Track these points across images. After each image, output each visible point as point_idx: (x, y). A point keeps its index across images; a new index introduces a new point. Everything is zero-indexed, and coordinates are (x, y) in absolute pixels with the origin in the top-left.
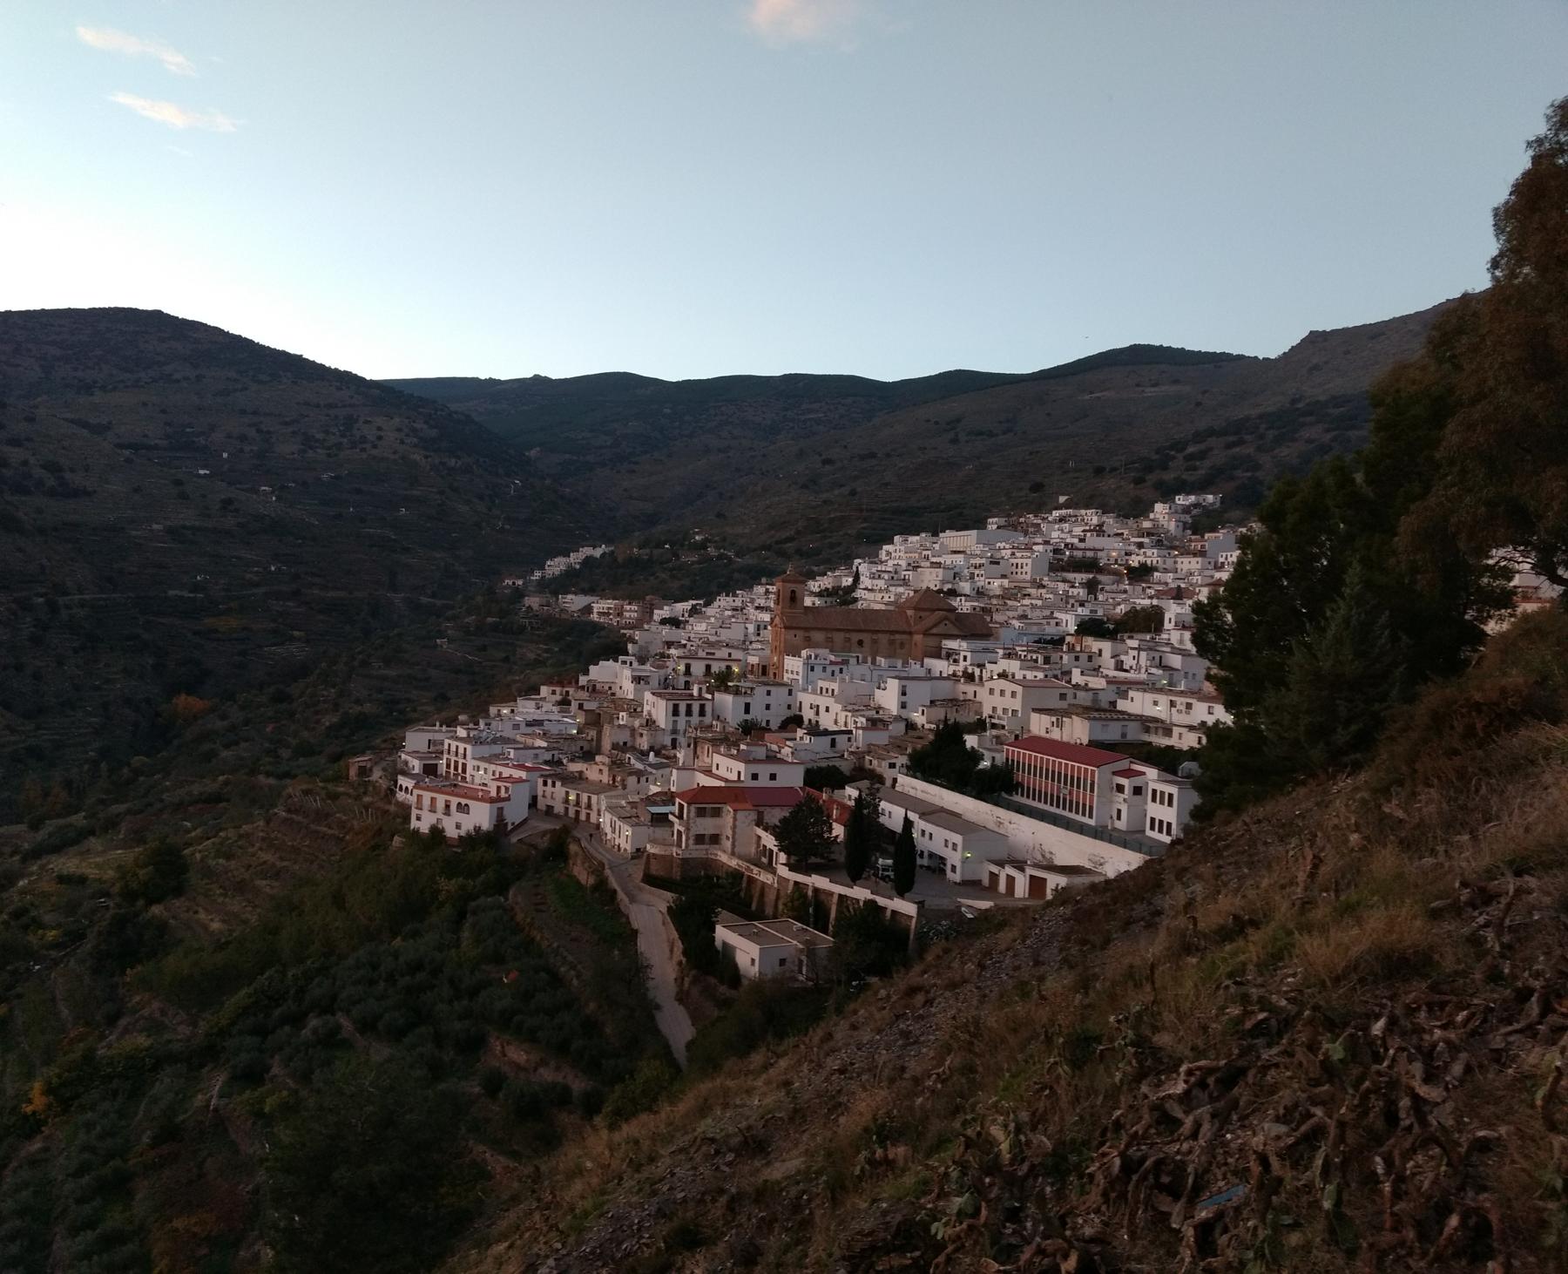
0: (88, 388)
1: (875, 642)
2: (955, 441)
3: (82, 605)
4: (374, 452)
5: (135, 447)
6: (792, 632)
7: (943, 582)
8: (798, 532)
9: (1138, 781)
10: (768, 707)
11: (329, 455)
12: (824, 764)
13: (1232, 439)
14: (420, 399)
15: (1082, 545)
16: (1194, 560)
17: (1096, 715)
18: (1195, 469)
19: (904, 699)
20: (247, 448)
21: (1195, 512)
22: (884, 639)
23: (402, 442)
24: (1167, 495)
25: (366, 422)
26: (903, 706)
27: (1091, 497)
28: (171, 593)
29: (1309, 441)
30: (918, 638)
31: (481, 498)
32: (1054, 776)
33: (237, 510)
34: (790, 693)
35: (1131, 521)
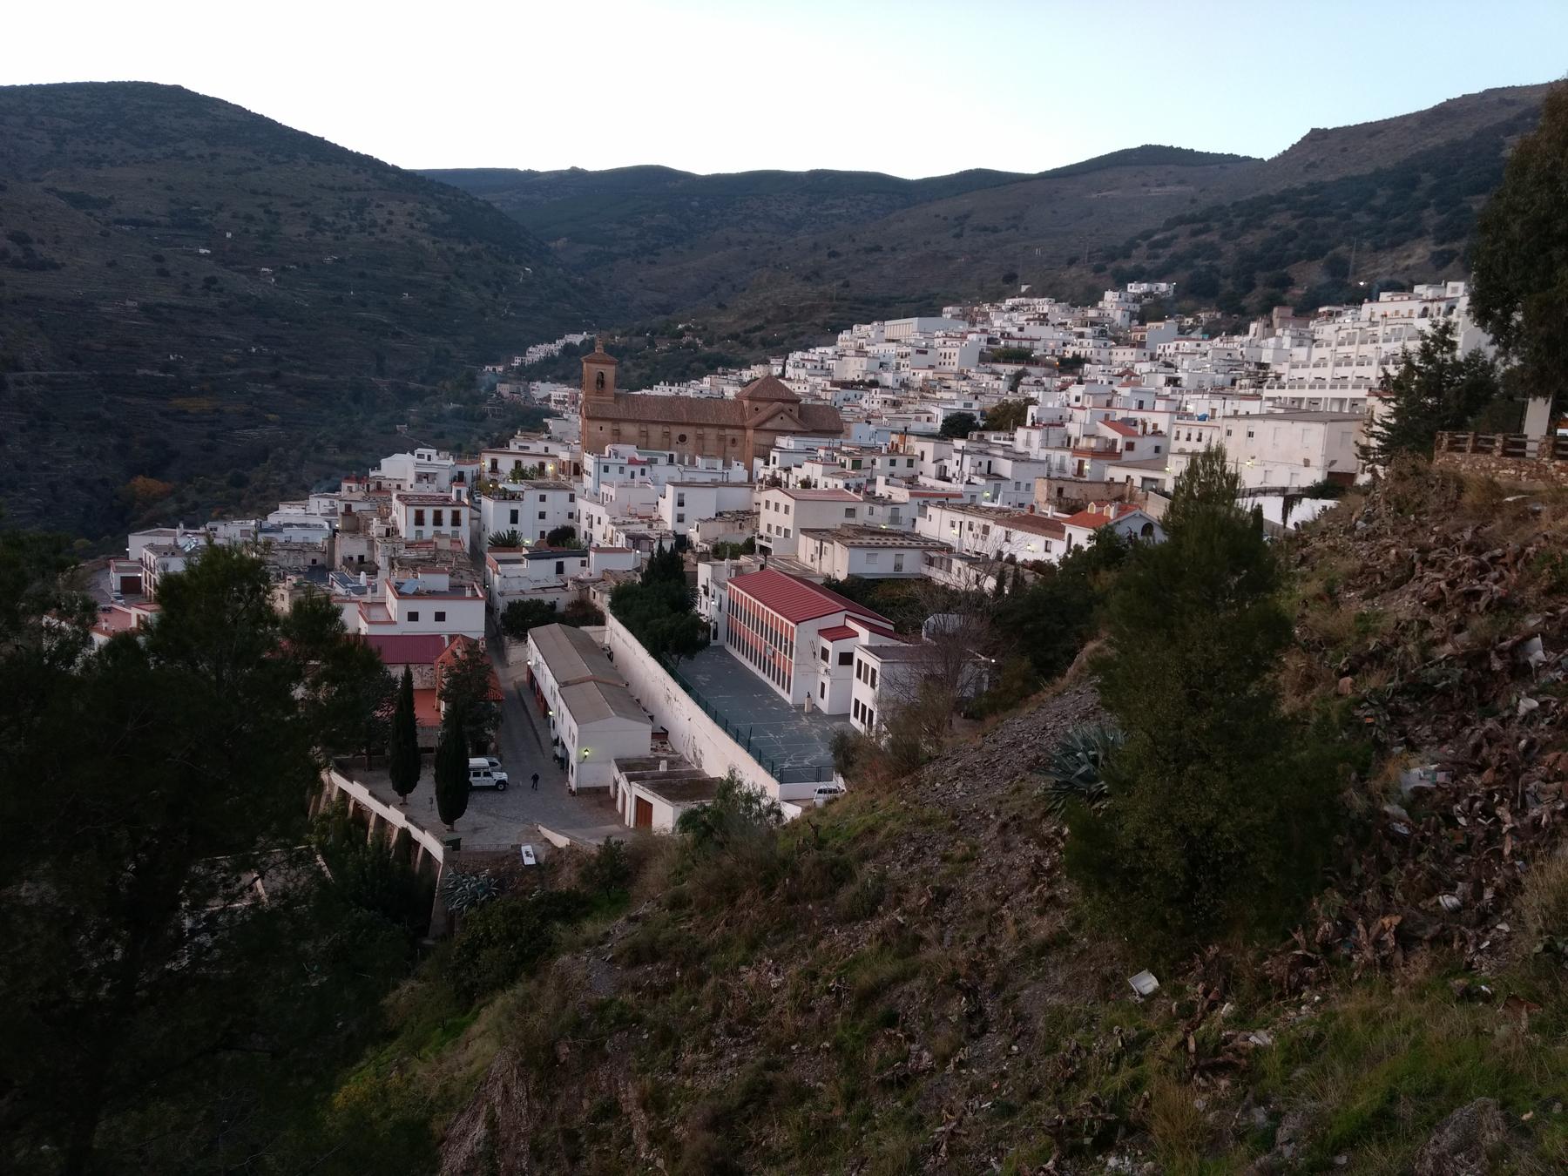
0: (97, 163)
1: (700, 437)
2: (958, 236)
3: (37, 381)
4: (382, 236)
5: (136, 223)
6: (598, 424)
7: (866, 373)
8: (768, 321)
9: (845, 645)
10: (542, 516)
11: (337, 238)
12: (526, 599)
13: (1201, 226)
14: (441, 184)
15: (1019, 335)
16: (1129, 351)
17: (866, 540)
18: (1157, 257)
19: (681, 510)
20: (253, 229)
21: (1145, 301)
22: (711, 434)
23: (412, 227)
24: (1120, 284)
25: (379, 206)
26: (680, 519)
27: (1051, 286)
28: (140, 372)
29: (1275, 228)
30: (750, 433)
31: (487, 284)
32: (763, 629)
33: (221, 290)
34: (572, 498)
35: (1078, 311)
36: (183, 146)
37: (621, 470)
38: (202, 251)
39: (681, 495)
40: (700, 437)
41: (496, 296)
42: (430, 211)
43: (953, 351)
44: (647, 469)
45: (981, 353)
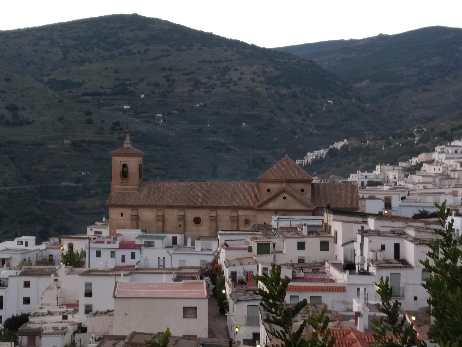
1: (215, 219)
4: (234, 88)
25: (236, 70)
28: (63, 184)
31: (299, 113)
36: (131, 47)
37: (113, 254)
38: (125, 107)
39: (88, 285)
40: (215, 219)
41: (304, 120)
42: (268, 70)
44: (137, 252)
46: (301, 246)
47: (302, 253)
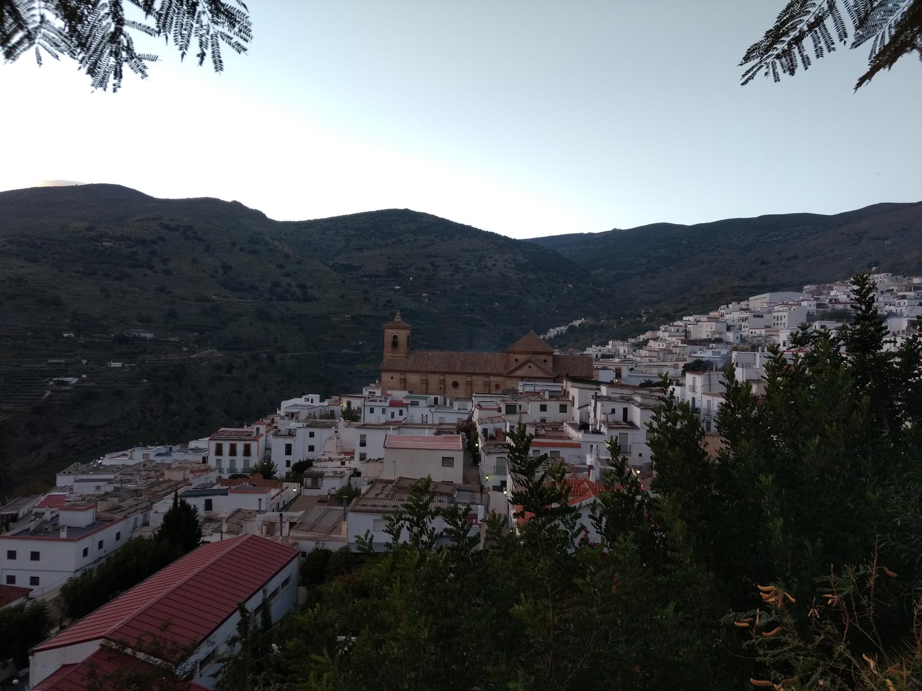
1: (470, 384)
5: (369, 276)
22: (479, 381)
23: (506, 267)
25: (490, 257)
28: (343, 351)
37: (384, 411)
39: (363, 436)
40: (470, 384)
41: (548, 301)
43: (782, 314)
44: (404, 410)
45: (808, 314)
46: (543, 408)
47: (544, 414)
